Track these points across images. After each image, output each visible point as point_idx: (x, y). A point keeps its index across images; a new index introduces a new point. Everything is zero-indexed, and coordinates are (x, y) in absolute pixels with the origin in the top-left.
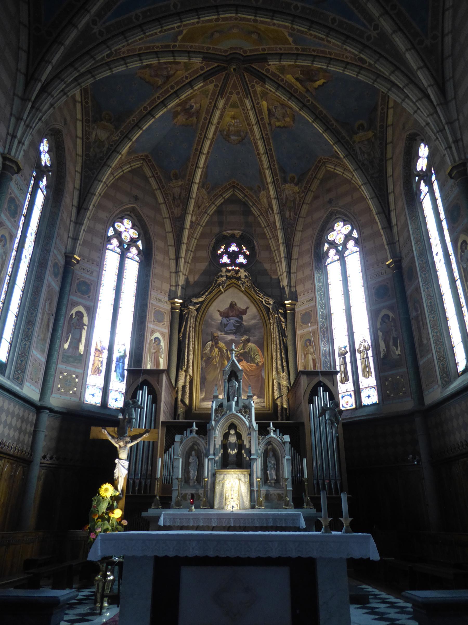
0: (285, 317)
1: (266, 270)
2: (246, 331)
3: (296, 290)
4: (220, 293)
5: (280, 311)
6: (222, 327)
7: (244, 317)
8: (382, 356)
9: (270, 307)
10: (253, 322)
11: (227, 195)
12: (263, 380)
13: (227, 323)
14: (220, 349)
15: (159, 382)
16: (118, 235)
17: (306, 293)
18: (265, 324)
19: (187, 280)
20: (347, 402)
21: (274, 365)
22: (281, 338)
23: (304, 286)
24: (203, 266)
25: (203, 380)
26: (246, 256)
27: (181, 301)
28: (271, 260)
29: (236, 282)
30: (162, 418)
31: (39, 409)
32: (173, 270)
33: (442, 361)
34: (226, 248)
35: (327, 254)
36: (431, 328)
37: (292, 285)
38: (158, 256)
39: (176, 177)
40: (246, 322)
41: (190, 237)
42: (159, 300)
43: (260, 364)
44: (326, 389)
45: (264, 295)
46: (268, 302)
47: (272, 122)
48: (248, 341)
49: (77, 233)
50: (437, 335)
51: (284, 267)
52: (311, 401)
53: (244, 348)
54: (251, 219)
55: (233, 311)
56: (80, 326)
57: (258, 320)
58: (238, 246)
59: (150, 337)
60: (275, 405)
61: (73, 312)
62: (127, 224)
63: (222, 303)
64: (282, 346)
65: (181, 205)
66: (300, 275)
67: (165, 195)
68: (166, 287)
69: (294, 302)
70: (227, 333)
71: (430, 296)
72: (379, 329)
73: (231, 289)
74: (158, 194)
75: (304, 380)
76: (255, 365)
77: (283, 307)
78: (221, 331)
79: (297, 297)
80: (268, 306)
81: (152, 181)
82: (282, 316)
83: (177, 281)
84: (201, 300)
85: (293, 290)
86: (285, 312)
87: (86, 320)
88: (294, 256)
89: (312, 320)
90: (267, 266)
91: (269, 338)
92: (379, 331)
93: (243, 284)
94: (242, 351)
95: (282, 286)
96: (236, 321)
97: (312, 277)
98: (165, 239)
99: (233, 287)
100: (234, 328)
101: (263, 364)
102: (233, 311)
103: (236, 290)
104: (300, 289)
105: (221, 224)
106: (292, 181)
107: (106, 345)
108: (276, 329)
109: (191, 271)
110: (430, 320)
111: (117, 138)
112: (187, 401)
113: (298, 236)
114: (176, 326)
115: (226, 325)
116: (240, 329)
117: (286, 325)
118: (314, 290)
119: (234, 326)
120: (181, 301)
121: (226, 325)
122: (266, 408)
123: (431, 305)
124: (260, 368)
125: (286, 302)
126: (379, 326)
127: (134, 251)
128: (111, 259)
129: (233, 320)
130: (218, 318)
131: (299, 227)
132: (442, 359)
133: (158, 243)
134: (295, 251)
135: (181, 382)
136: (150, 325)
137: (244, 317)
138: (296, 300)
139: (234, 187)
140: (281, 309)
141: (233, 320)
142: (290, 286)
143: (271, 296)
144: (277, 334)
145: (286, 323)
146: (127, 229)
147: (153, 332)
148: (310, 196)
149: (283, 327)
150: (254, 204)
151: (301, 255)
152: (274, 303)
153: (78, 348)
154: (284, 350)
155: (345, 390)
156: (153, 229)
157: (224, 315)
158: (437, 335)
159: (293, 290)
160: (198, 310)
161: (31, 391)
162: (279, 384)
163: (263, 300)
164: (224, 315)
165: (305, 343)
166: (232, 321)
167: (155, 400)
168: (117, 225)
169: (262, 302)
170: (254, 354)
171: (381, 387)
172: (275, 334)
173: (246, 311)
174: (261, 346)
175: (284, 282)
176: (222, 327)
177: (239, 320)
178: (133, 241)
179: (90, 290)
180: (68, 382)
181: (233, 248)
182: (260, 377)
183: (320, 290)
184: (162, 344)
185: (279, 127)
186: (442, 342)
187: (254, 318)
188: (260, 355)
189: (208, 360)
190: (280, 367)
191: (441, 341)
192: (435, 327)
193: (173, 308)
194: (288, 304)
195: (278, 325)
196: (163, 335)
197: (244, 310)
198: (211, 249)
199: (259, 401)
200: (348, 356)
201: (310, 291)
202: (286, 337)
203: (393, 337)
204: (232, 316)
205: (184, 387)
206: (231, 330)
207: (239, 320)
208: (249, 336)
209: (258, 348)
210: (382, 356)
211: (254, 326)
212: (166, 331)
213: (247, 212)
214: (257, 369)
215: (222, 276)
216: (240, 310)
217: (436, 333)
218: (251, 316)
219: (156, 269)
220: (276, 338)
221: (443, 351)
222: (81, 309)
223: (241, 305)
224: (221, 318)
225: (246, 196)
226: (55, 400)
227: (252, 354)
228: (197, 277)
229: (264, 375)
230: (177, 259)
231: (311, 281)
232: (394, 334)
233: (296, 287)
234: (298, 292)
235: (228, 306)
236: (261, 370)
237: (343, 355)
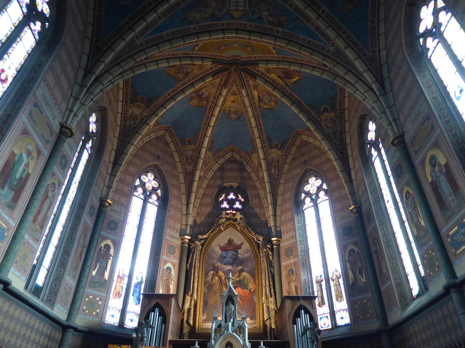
0: (272, 251)
1: (257, 214)
3: (280, 230)
4: (220, 231)
5: (268, 246)
6: (222, 259)
7: (239, 251)
9: (260, 243)
10: (246, 255)
11: (228, 156)
14: (220, 278)
15: (169, 305)
16: (143, 185)
17: (288, 232)
18: (256, 256)
19: (195, 221)
20: (324, 323)
21: (264, 291)
24: (207, 210)
25: (206, 304)
26: (241, 203)
27: (189, 238)
28: (261, 206)
29: (233, 223)
30: (170, 337)
31: (64, 328)
32: (184, 212)
34: (226, 197)
35: (303, 202)
37: (277, 225)
38: (173, 202)
39: (190, 143)
40: (241, 255)
41: (199, 187)
42: (172, 236)
43: (252, 290)
44: (307, 312)
45: (255, 233)
47: (261, 105)
48: (242, 271)
49: (111, 182)
51: (271, 212)
52: (295, 322)
53: (239, 276)
54: (245, 174)
55: (231, 246)
56: (107, 256)
58: (235, 194)
59: (163, 267)
60: (265, 326)
61: (103, 245)
62: (151, 176)
63: (222, 239)
64: (270, 275)
65: (192, 164)
66: (283, 218)
67: (181, 156)
68: (178, 226)
69: (279, 239)
70: (225, 264)
74: (175, 155)
75: (288, 303)
76: (248, 291)
77: (270, 245)
78: (221, 263)
79: (281, 235)
81: (171, 145)
83: (187, 221)
84: (205, 237)
85: (278, 229)
87: (112, 251)
88: (279, 203)
89: (294, 253)
90: (257, 210)
93: (239, 225)
94: (238, 279)
97: (292, 219)
98: (179, 189)
100: (231, 260)
101: (255, 290)
102: (231, 246)
104: (283, 229)
105: (222, 178)
106: (276, 147)
107: (127, 273)
108: (265, 261)
109: (198, 214)
110: (387, 254)
111: (147, 114)
112: (191, 322)
113: (281, 188)
114: (185, 258)
115: (225, 258)
116: (236, 261)
117: (273, 258)
118: (294, 229)
119: (232, 258)
120: (189, 238)
121: (225, 258)
123: (387, 242)
125: (273, 239)
126: (347, 259)
127: (154, 197)
128: (136, 203)
129: (230, 254)
130: (219, 251)
131: (282, 181)
133: (173, 192)
134: (280, 199)
135: (187, 306)
136: (164, 257)
137: (239, 251)
138: (281, 237)
139: (233, 150)
141: (230, 254)
142: (276, 226)
144: (266, 265)
145: (273, 256)
146: (150, 181)
147: (166, 262)
148: (290, 158)
150: (248, 164)
151: (284, 202)
152: (263, 239)
153: (103, 275)
154: (272, 278)
155: (322, 312)
156: (170, 181)
157: (224, 249)
159: (278, 229)
160: (202, 245)
161: (60, 312)
162: (268, 307)
163: (255, 238)
164: (224, 249)
165: (289, 273)
167: (165, 321)
168: (143, 177)
169: (254, 239)
170: (247, 282)
171: (352, 310)
172: (264, 265)
174: (253, 276)
175: (271, 223)
176: (222, 259)
178: (154, 190)
179: (117, 227)
180: (92, 305)
181: (232, 196)
184: (173, 272)
185: (267, 108)
187: (247, 252)
189: (210, 287)
190: (268, 293)
193: (183, 243)
194: (275, 241)
196: (174, 265)
198: (214, 197)
200: (323, 284)
202: (273, 268)
203: (359, 268)
205: (189, 310)
206: (229, 262)
208: (244, 267)
211: (247, 259)
212: (176, 262)
213: (242, 169)
214: (250, 294)
215: (222, 218)
217: (393, 264)
218: (245, 251)
219: (171, 212)
222: (109, 242)
224: (221, 252)
225: (242, 157)
226: (80, 321)
228: (203, 219)
229: (256, 299)
230: (188, 204)
231: (292, 223)
232: (359, 265)
237: (319, 282)
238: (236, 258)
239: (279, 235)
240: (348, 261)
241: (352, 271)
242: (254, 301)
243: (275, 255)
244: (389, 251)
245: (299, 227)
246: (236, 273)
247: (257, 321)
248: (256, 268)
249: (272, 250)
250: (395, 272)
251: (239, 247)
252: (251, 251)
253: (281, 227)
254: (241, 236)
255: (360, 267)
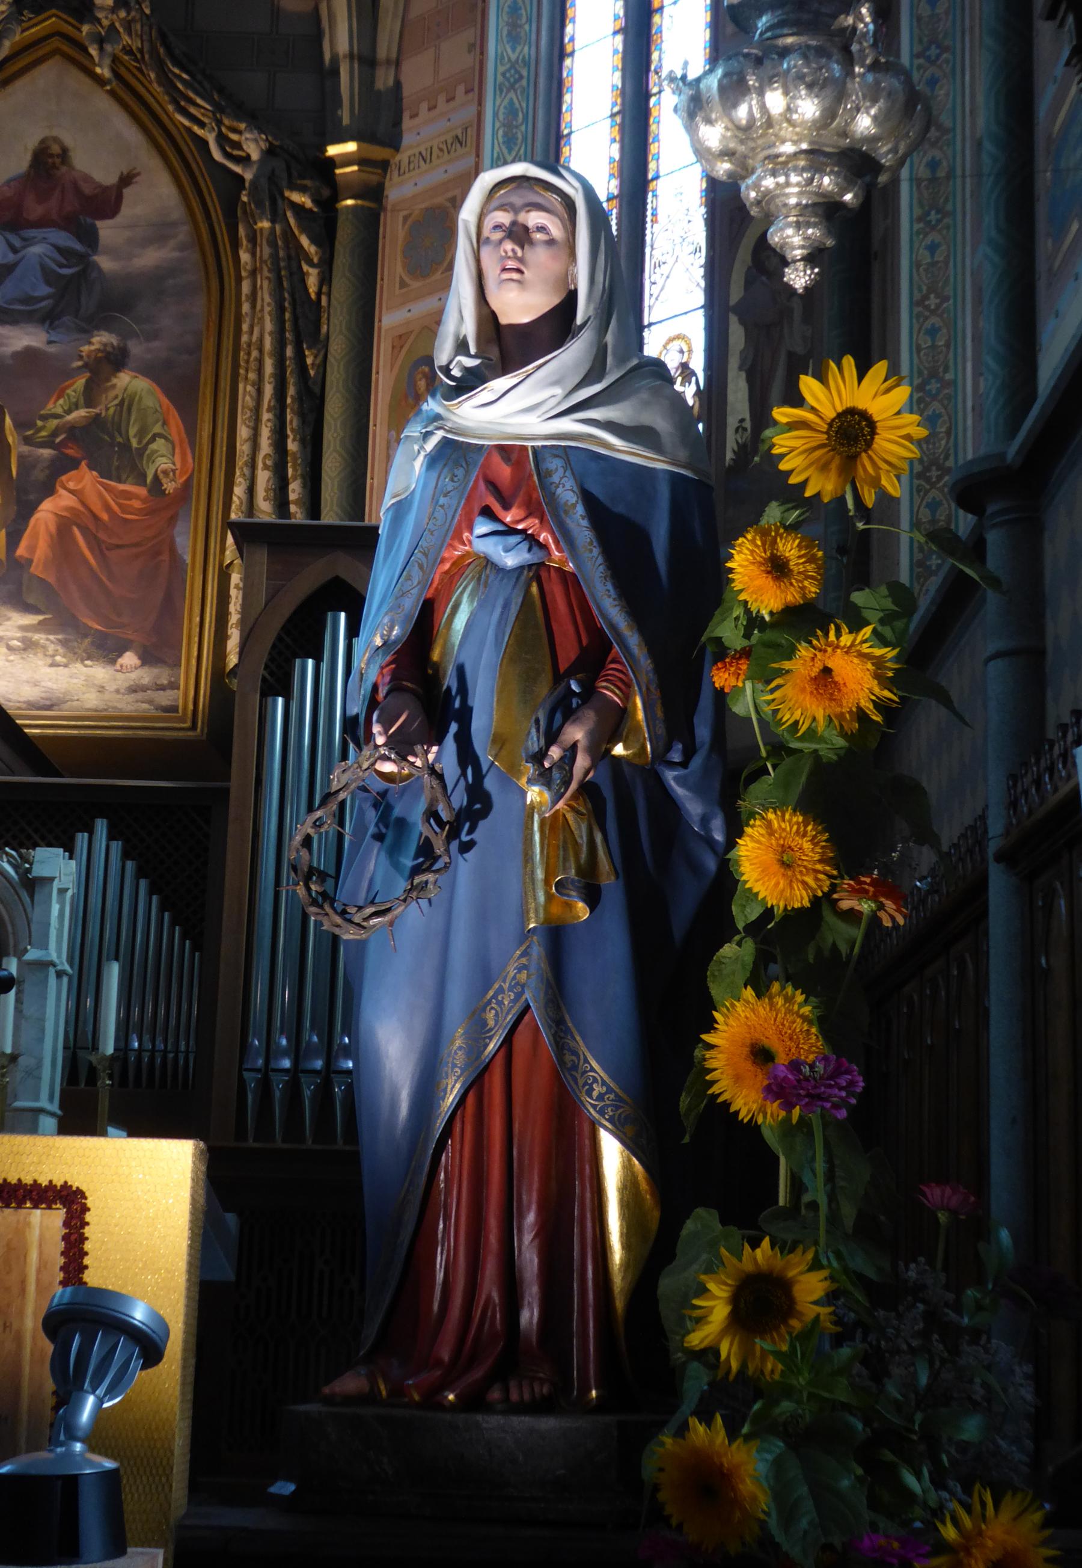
0: (326, 238)
2: (115, 305)
3: (398, 84)
5: (297, 197)
8: (729, 455)
9: (248, 176)
10: (150, 258)
12: (177, 564)
13: (11, 257)
17: (441, 99)
21: (239, 491)
22: (289, 351)
23: (437, 59)
29: (69, 30)
33: (933, 485)
36: (912, 304)
37: (382, 53)
40: (114, 253)
43: (169, 486)
45: (218, 108)
46: (238, 145)
48: (116, 360)
50: (933, 347)
53: (90, 397)
57: (182, 248)
64: (291, 391)
69: (378, 152)
71: (939, 127)
72: (736, 310)
73: (44, 67)
76: (142, 491)
79: (397, 123)
80: (237, 169)
82: (304, 230)
85: (384, 79)
86: (328, 205)
91: (228, 344)
92: (733, 319)
93: (101, 42)
94: (82, 412)
95: (327, 57)
96: (59, 249)
99: (58, 57)
100: (44, 290)
101: (187, 486)
103: (76, 79)
104: (416, 77)
110: (915, 265)
116: (76, 297)
117: (326, 279)
118: (475, 85)
119: (49, 276)
122: (183, 720)
123: (933, 180)
124: (166, 505)
125: (333, 150)
126: (736, 293)
132: (934, 473)
138: (394, 142)
140: (303, 190)
142: (367, 60)
143: (255, 119)
144: (269, 326)
149: (312, 290)
152: (270, 152)
154: (302, 414)
158: (933, 347)
163: (211, 139)
165: (412, 383)
166: (36, 250)
169: (204, 143)
170: (142, 433)
172: (260, 327)
173: (119, 198)
174: (182, 389)
177: (78, 247)
182: (165, 557)
183: (509, 84)
186: (953, 383)
188: (175, 438)
191: (949, 376)
192: (933, 301)
194: (347, 160)
195: (279, 279)
197: (105, 189)
199: (146, 681)
201: (461, 89)
202: (322, 345)
203: (791, 355)
204: (40, 224)
206: (28, 300)
207: (78, 247)
208: (125, 335)
209: (165, 401)
210: (729, 455)
211: (156, 282)
214: (151, 512)
216: (87, 190)
217: (933, 332)
218: (144, 229)
220: (261, 350)
221: (948, 433)
223: (94, 165)
227: (132, 431)
231: (470, 35)
233: (398, 64)
234: (407, 91)
235: (21, 163)
236: (172, 520)
238: (83, 274)
239: (382, 125)
240: (743, 311)
241: (750, 380)
242: (173, 550)
243: (342, 260)
244: (932, 248)
245: (513, 65)
246: (71, 374)
247: (185, 675)
248: (209, 346)
249: (324, 223)
250: (933, 386)
251: (107, 202)
252: (183, 233)
253: (406, 67)
254: (122, 125)
255: (800, 350)
